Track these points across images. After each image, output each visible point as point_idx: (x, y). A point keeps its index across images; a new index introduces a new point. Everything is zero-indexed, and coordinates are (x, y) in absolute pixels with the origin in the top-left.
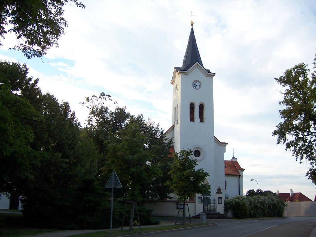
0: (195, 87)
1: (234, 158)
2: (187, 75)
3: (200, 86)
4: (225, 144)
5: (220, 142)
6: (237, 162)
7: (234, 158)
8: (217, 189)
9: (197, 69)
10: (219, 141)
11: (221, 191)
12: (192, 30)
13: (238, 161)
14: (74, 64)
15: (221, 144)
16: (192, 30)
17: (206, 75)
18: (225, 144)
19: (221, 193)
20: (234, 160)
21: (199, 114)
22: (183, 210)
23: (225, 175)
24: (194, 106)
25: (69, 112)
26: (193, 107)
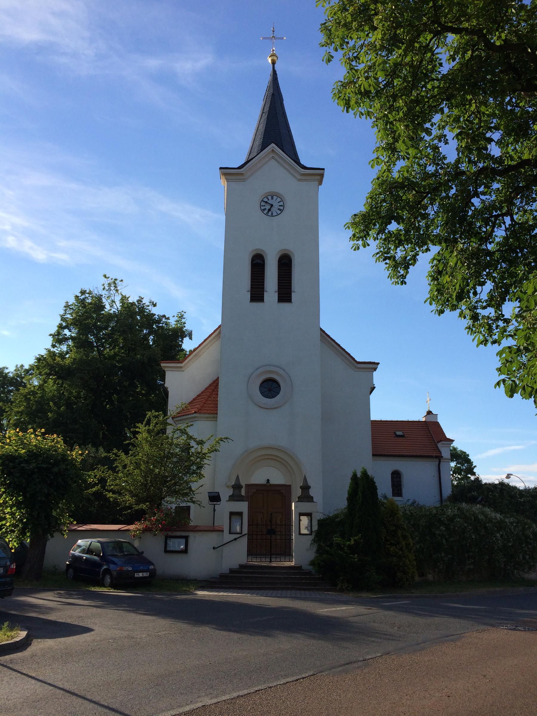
0: (270, 214)
1: (429, 413)
2: (244, 180)
3: (282, 208)
4: (373, 366)
5: (358, 359)
6: (437, 425)
7: (429, 413)
8: (301, 487)
9: (273, 162)
10: (354, 359)
11: (312, 492)
12: (274, 72)
13: (440, 420)
14: (411, 267)
15: (359, 365)
16: (274, 72)
17: (299, 177)
18: (373, 366)
19: (310, 499)
20: (431, 419)
21: (279, 283)
22: (269, 541)
23: (373, 455)
24: (264, 261)
25: (142, 310)
26: (261, 262)
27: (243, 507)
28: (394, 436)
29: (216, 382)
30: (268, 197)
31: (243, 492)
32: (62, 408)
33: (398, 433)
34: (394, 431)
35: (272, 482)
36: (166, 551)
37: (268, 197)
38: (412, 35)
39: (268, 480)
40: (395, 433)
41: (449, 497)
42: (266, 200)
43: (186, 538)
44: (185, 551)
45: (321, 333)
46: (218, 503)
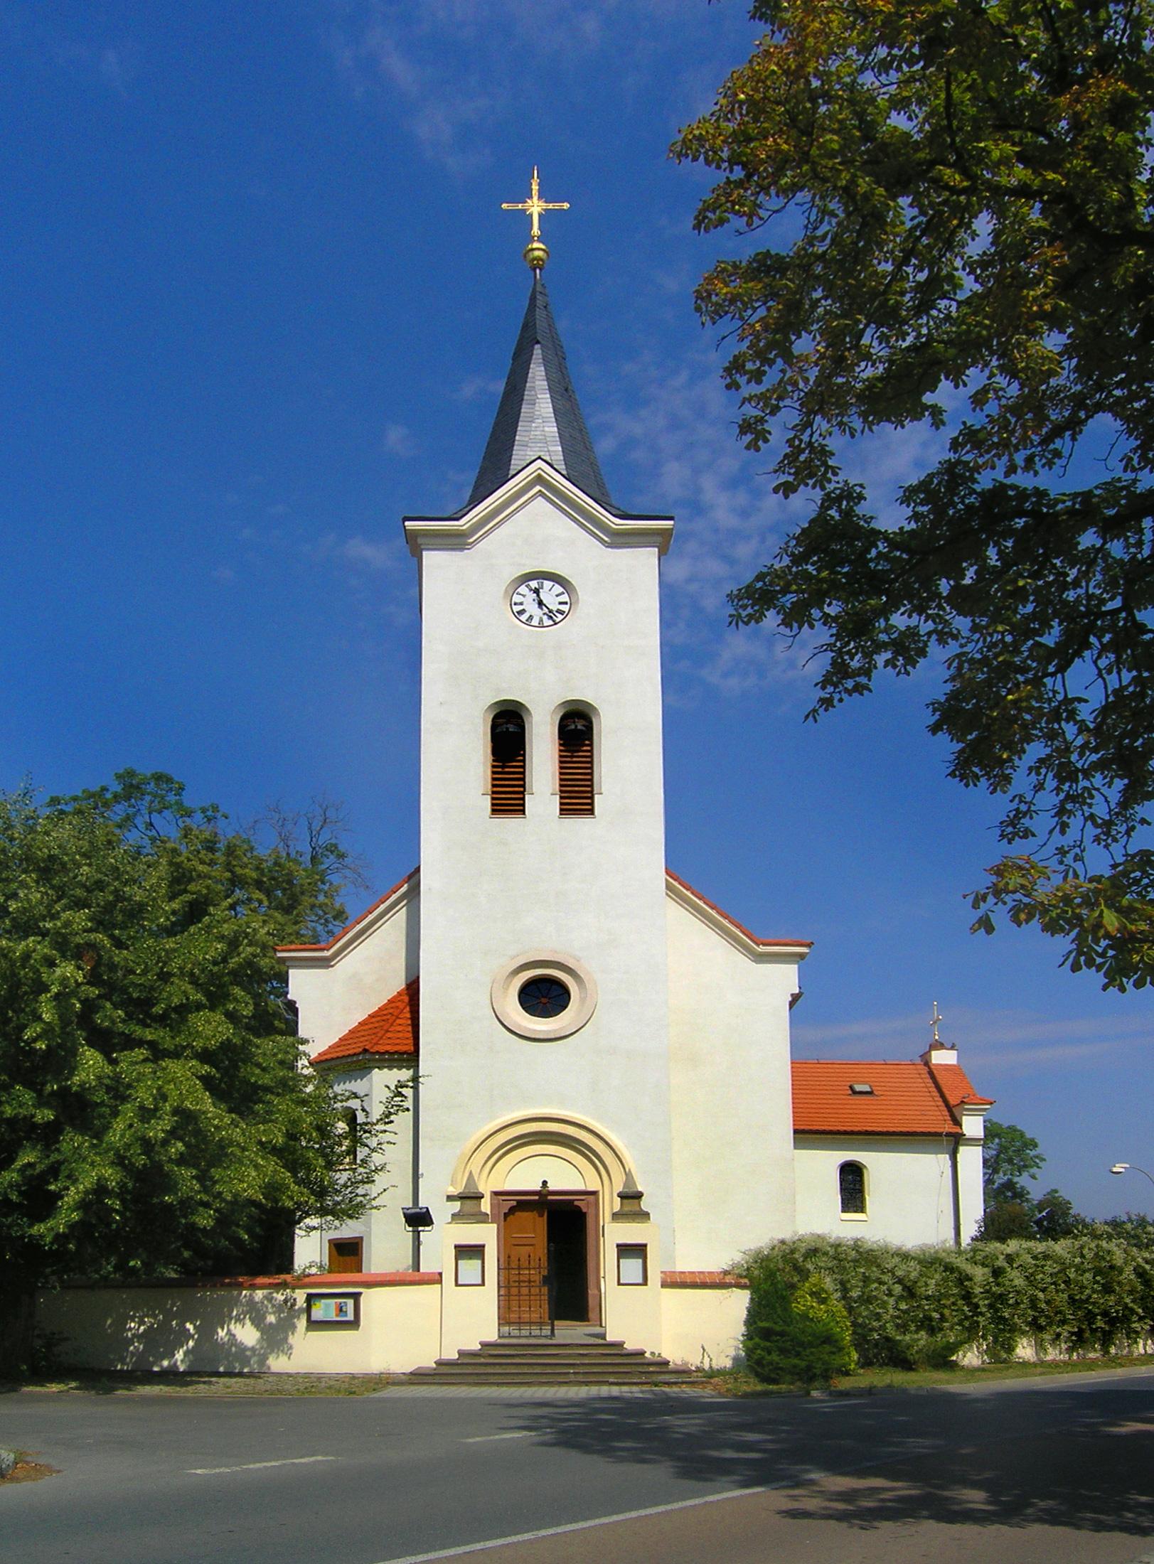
27: (487, 1235)
28: (850, 1092)
29: (414, 986)
30: (568, 606)
31: (486, 1206)
32: (904, 313)
33: (858, 1088)
34: (849, 1084)
35: (552, 1186)
36: (619, 1284)
37: (568, 606)
38: (946, 228)
39: (545, 1183)
40: (851, 1088)
41: (767, 1259)
42: (547, 622)
43: (356, 1297)
44: (354, 1324)
45: (666, 880)
46: (427, 1228)
